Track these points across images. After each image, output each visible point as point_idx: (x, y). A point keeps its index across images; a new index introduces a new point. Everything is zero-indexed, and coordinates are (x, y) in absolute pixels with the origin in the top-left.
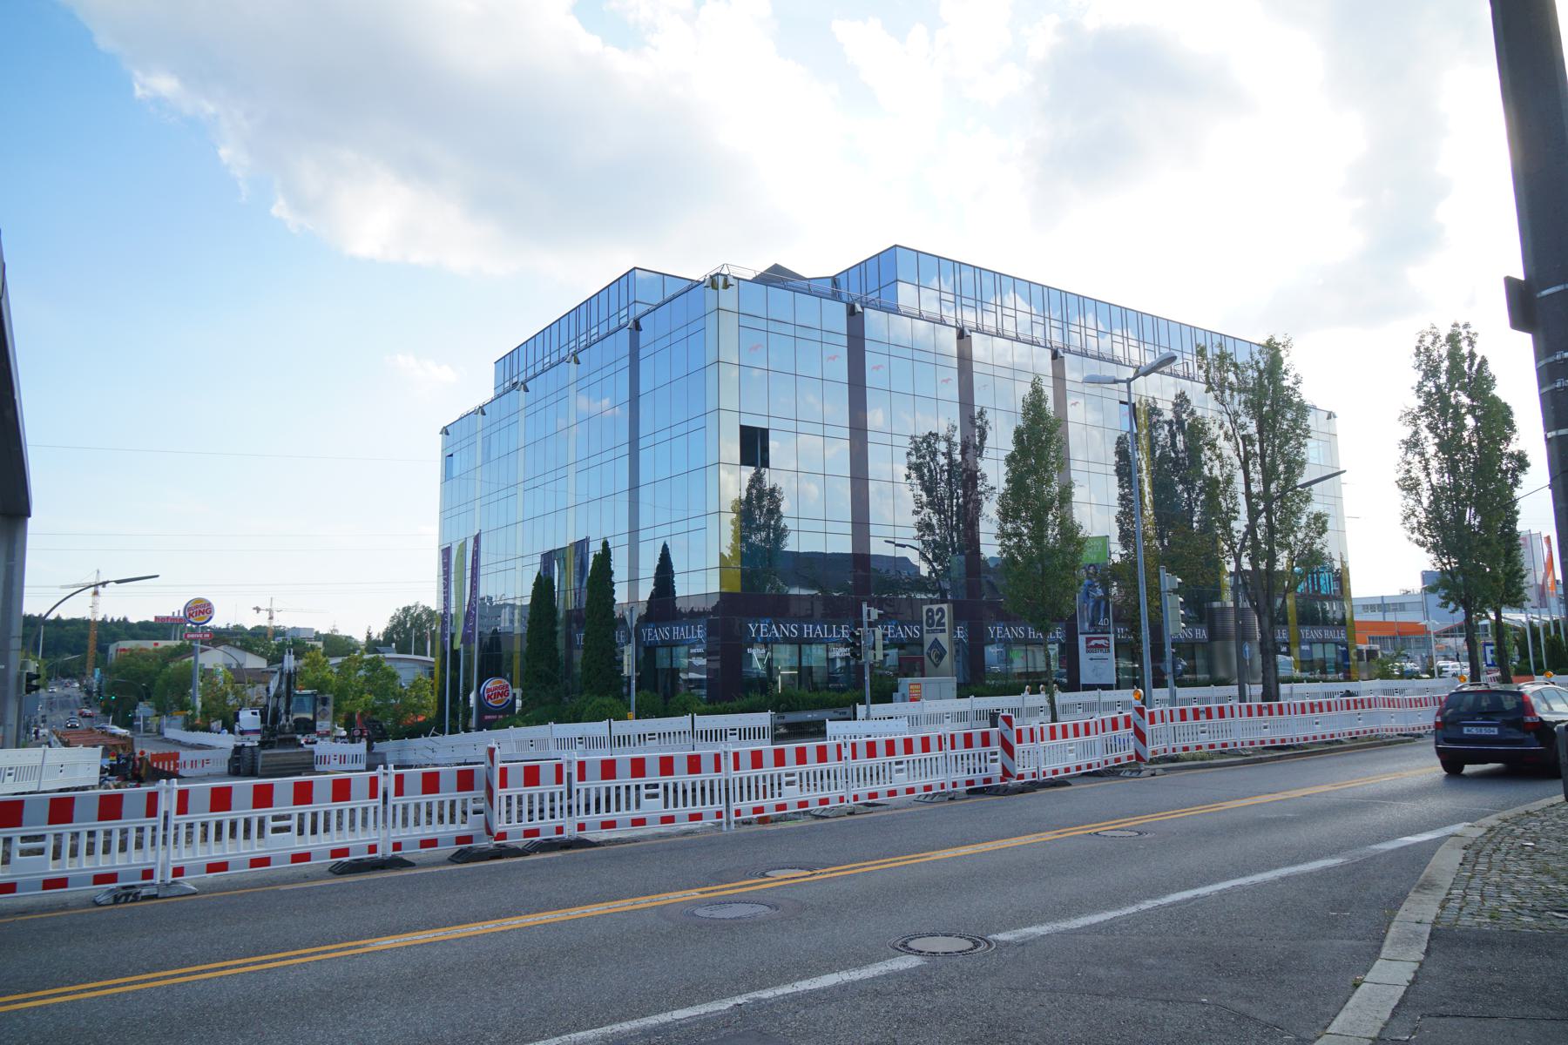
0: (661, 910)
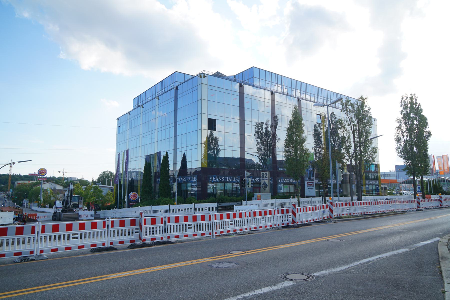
0: (201, 264)
